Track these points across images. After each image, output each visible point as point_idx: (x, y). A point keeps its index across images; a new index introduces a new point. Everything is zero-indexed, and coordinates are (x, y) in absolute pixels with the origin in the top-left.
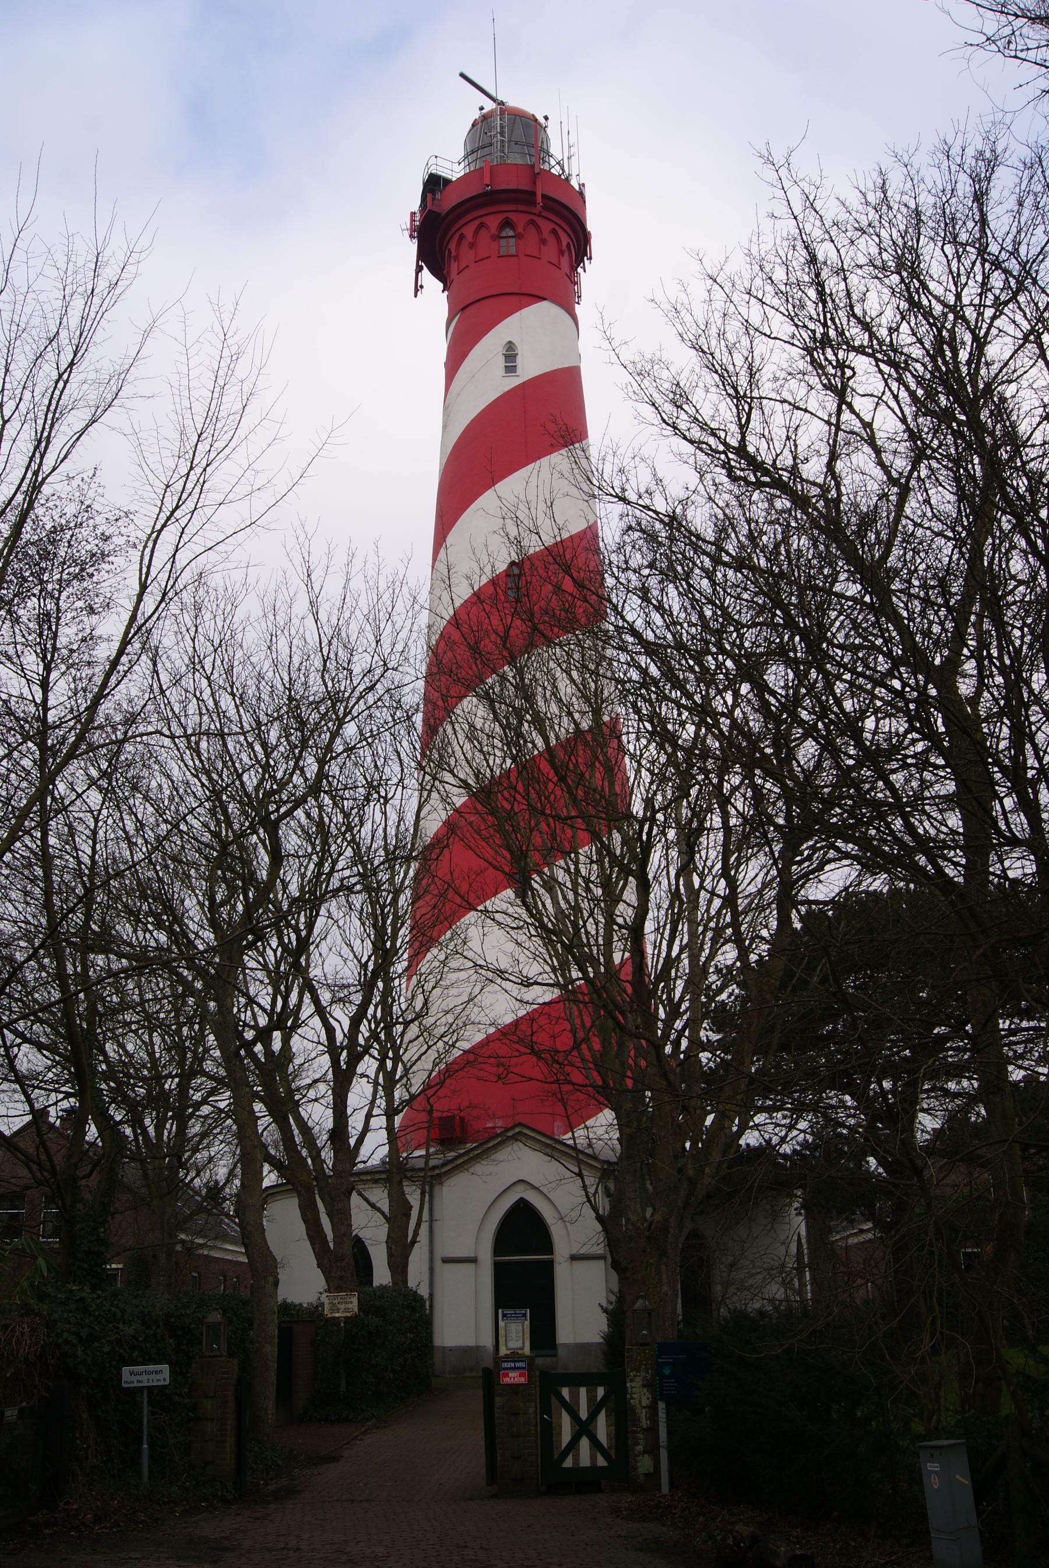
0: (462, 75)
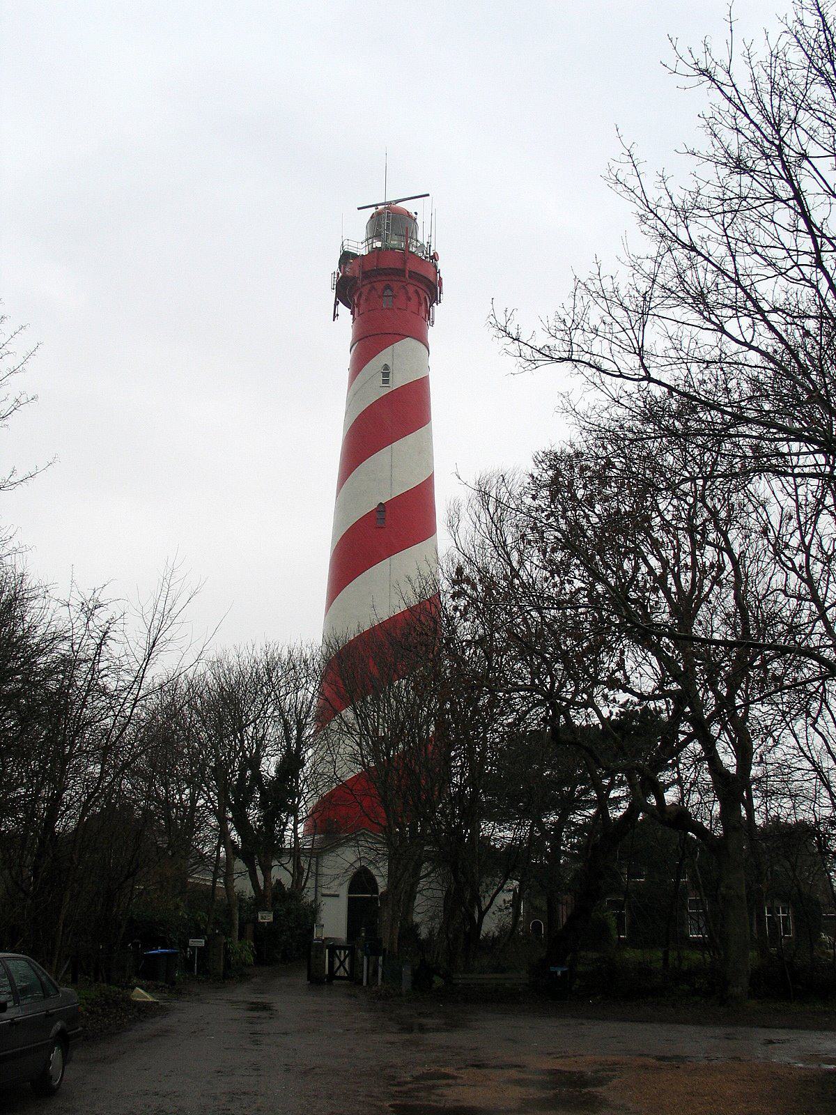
0: (359, 209)
